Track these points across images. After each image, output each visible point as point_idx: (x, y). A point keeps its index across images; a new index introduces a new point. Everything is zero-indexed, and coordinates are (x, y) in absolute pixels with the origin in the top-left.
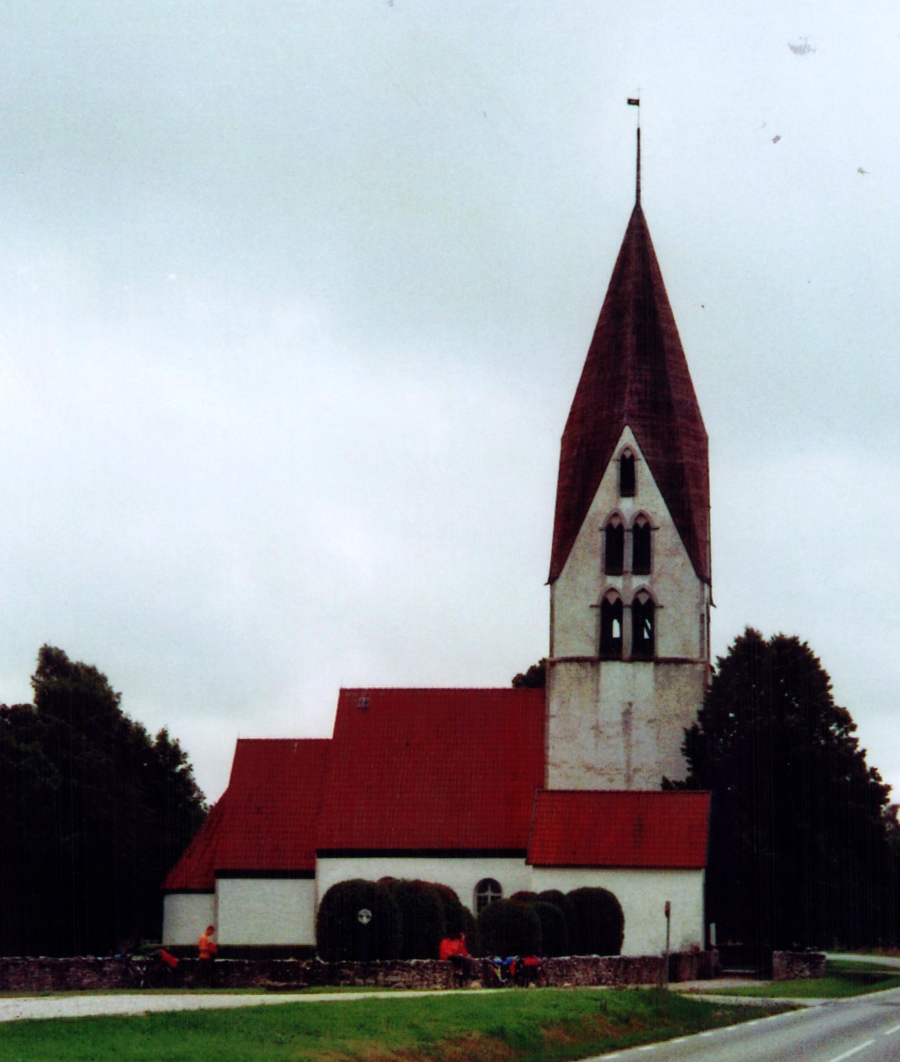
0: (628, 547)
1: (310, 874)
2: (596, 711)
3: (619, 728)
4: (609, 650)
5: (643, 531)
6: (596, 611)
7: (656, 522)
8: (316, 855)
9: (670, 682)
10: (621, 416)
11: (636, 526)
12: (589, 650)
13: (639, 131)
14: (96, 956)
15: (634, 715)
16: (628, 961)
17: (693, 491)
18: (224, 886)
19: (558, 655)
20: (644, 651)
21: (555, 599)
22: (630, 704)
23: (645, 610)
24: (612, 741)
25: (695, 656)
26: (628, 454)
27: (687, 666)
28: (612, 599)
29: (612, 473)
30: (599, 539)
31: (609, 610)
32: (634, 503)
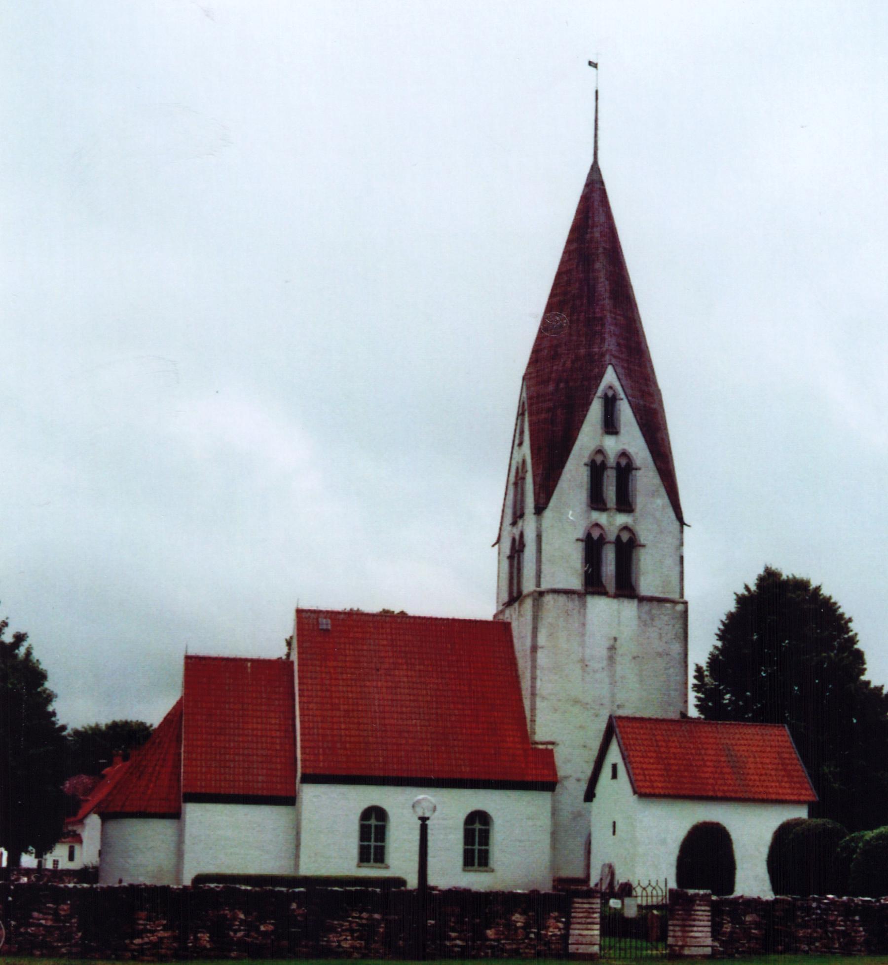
0: (612, 485)
2: (583, 644)
3: (604, 663)
4: (593, 584)
5: (625, 469)
6: (580, 546)
9: (652, 620)
10: (602, 355)
12: (576, 583)
13: (597, 92)
14: (91, 888)
15: (620, 651)
18: (193, 812)
19: (544, 586)
20: (626, 588)
22: (615, 639)
23: (628, 547)
24: (598, 676)
25: (676, 596)
26: (610, 393)
27: (668, 605)
28: (596, 535)
29: (596, 410)
31: (592, 546)
32: (616, 442)
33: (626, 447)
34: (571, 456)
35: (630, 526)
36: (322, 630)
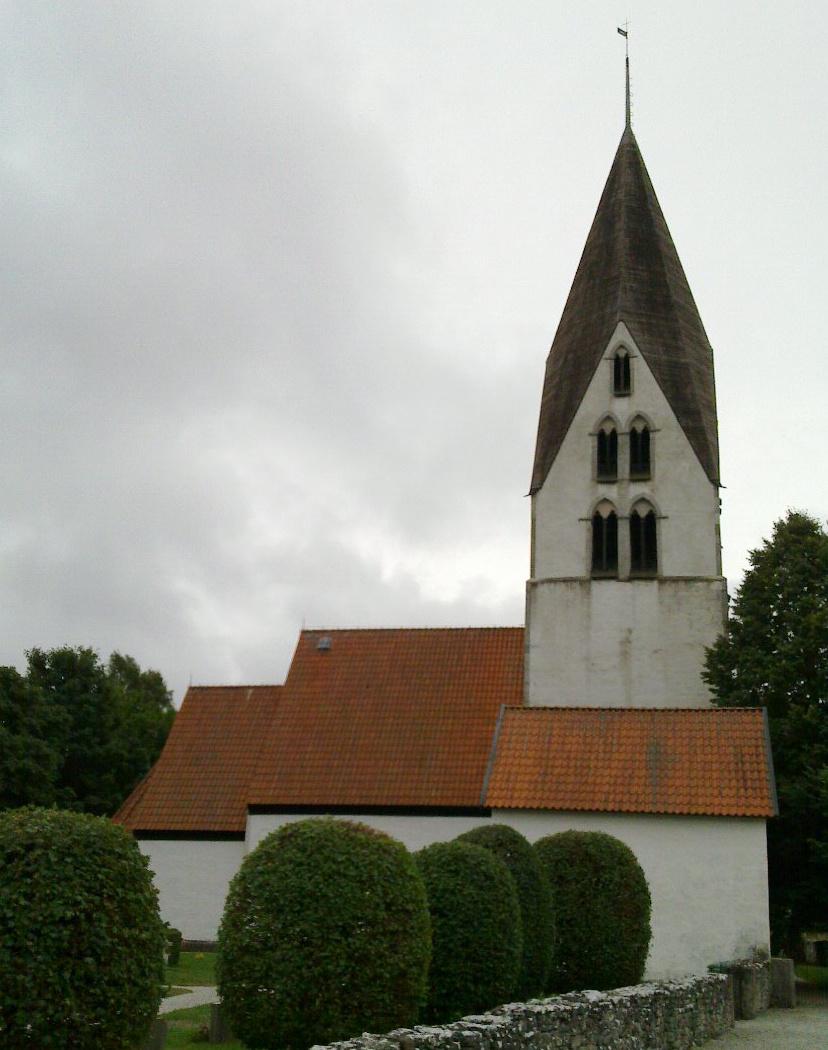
0: (624, 453)
1: (240, 836)
5: (641, 442)
6: (596, 438)
7: (656, 423)
8: (247, 811)
11: (633, 433)
16: (667, 1000)
17: (699, 392)
19: (538, 578)
21: (537, 512)
23: (645, 529)
25: (712, 574)
26: (622, 353)
27: (700, 584)
28: (605, 513)
30: (590, 447)
31: (603, 529)
33: (643, 409)
34: (573, 426)
35: (648, 498)
36: (320, 649)
